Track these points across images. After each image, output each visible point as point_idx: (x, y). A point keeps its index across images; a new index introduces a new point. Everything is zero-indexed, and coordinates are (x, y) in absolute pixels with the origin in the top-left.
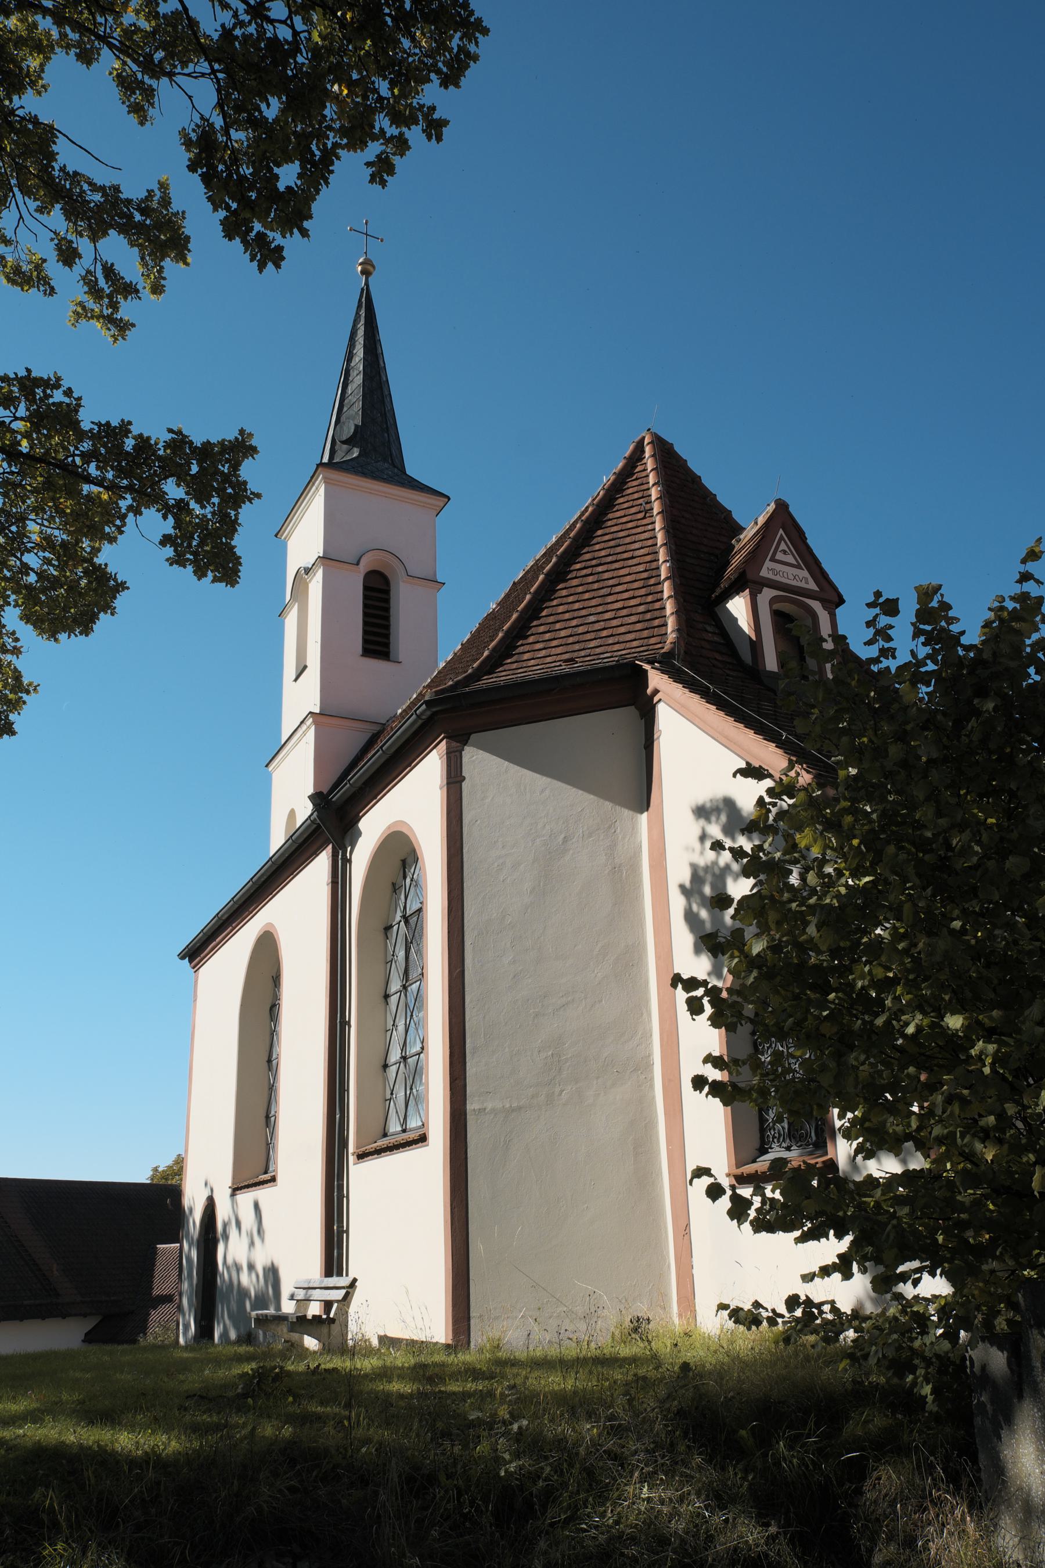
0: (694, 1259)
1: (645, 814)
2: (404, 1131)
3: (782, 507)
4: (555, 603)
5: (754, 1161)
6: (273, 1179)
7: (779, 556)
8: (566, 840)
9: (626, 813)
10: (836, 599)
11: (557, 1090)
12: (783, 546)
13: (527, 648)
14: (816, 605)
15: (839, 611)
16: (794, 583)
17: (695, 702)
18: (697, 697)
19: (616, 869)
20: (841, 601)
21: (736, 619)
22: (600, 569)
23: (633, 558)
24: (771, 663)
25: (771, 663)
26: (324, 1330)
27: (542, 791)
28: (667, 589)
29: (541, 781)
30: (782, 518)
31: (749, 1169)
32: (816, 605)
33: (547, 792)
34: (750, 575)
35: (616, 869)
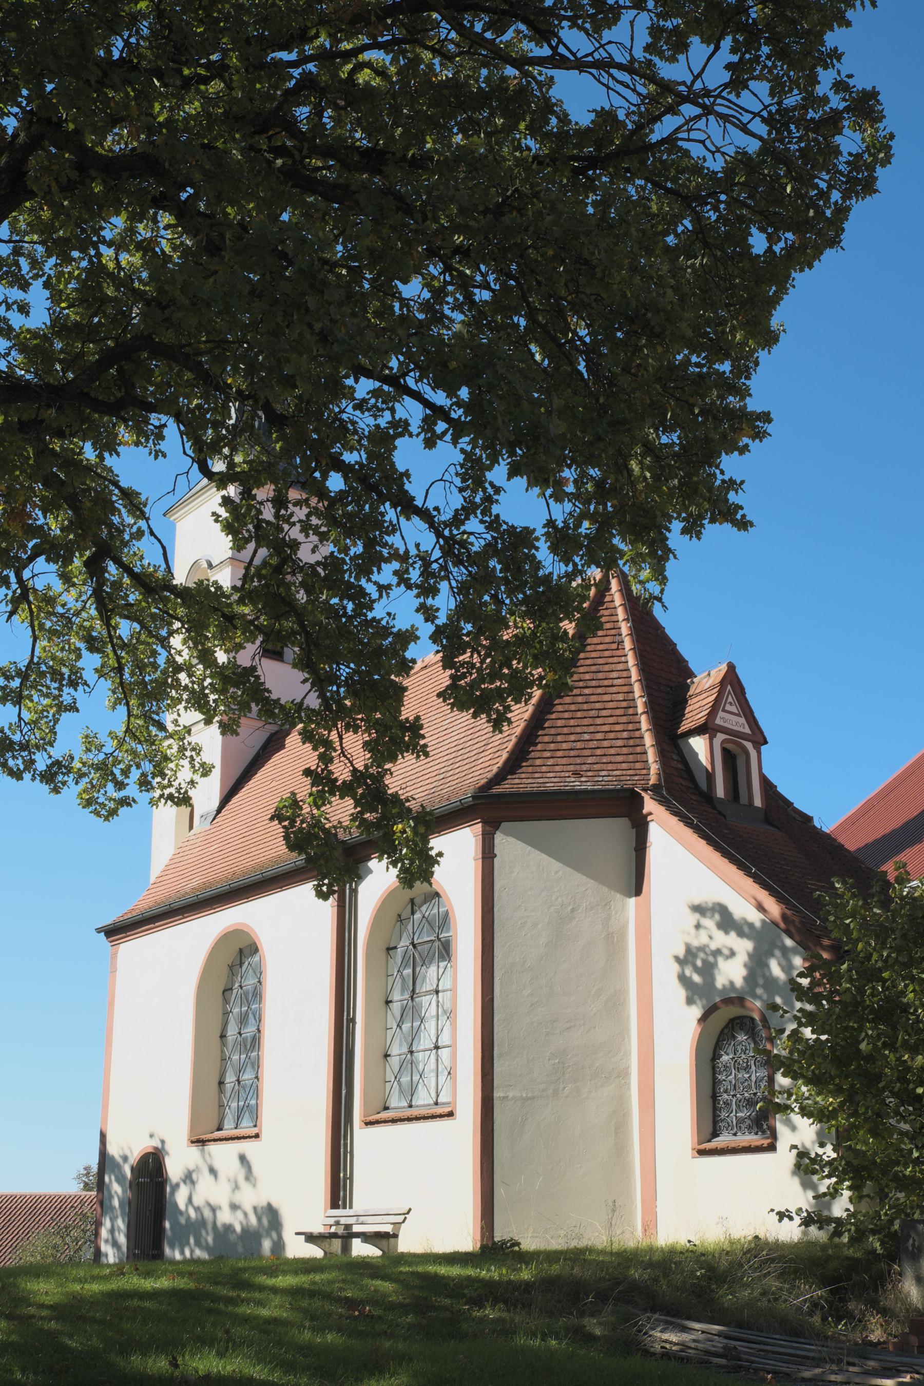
0: (658, 1203)
1: (633, 899)
2: (410, 1106)
3: (731, 668)
4: (553, 716)
5: (709, 1141)
6: (257, 1136)
7: (728, 707)
8: (573, 910)
9: (618, 896)
10: (762, 741)
11: (561, 1086)
12: (730, 699)
13: (538, 754)
14: (749, 745)
15: (763, 748)
16: (736, 728)
17: (673, 821)
18: (676, 819)
19: (609, 936)
20: (766, 742)
21: (697, 754)
22: (587, 691)
23: (612, 686)
24: (720, 792)
25: (720, 792)
26: (384, 1242)
27: (556, 872)
28: (644, 724)
29: (555, 865)
30: (731, 681)
31: (703, 1146)
32: (749, 745)
33: (560, 873)
34: (710, 725)
35: (609, 936)
